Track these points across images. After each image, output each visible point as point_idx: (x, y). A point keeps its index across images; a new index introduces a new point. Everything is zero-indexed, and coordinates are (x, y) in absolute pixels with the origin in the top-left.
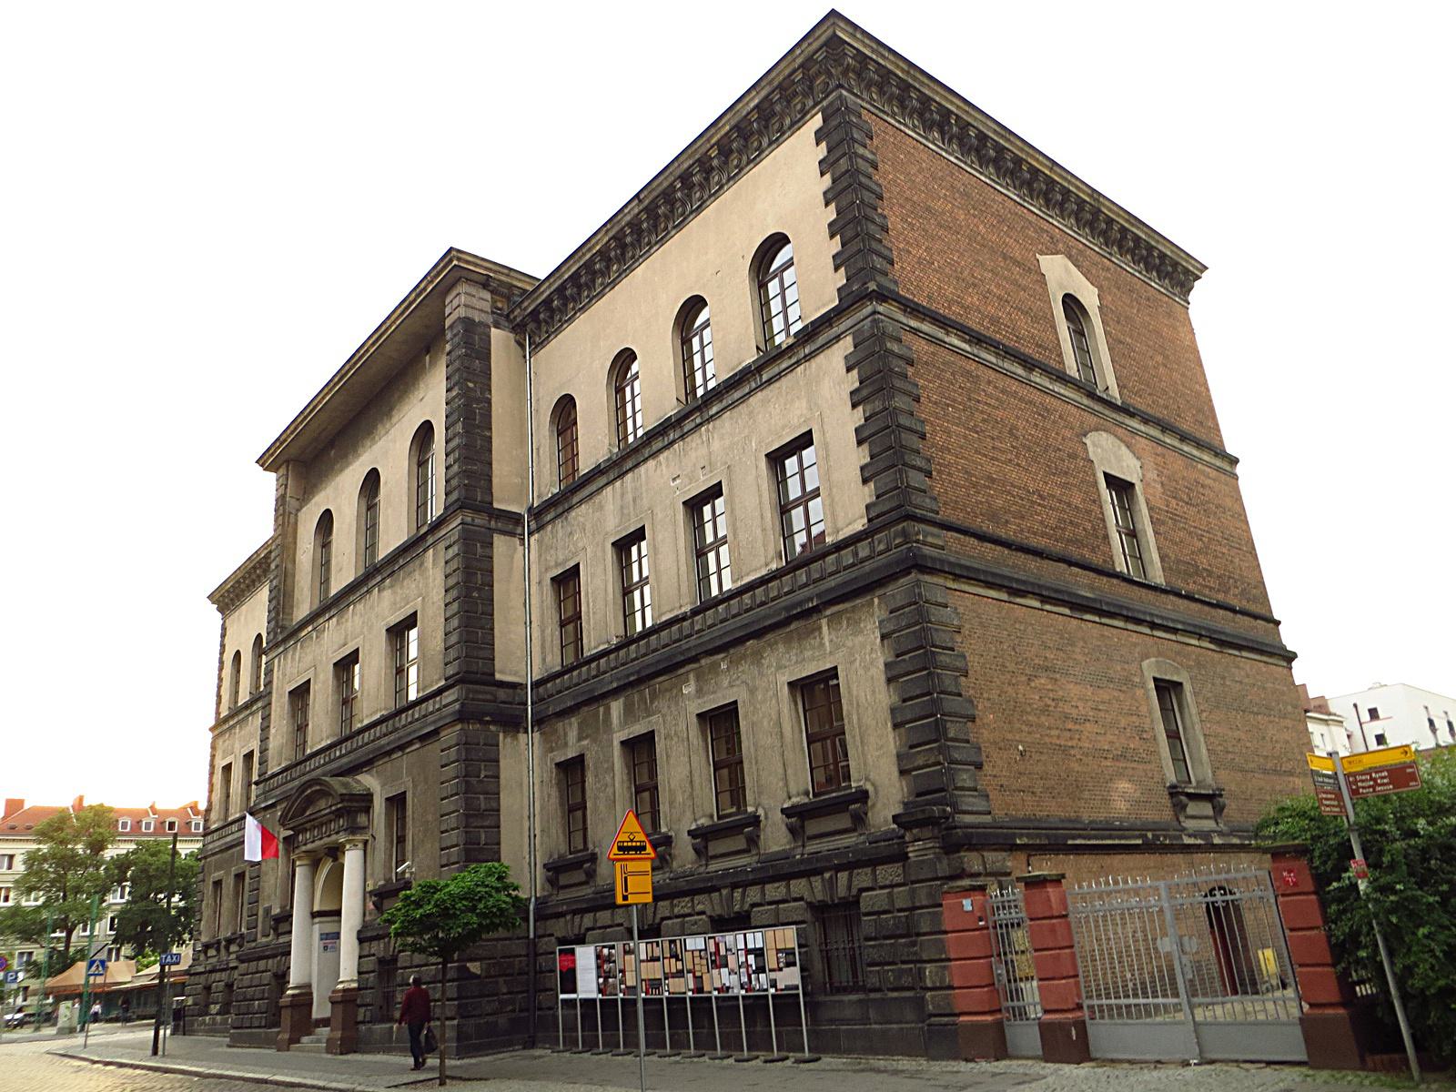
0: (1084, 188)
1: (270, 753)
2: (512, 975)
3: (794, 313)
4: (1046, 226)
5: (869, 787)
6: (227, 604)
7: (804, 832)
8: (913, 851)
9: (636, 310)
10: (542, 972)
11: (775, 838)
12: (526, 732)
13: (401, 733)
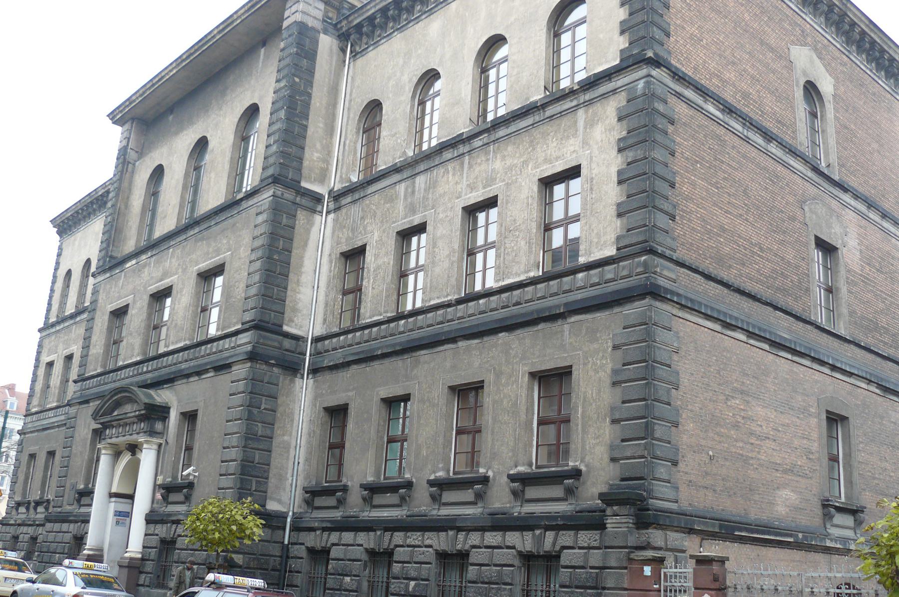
2: (267, 570)
3: (581, 63)
4: (799, 21)
5: (583, 468)
6: (65, 229)
7: (524, 494)
8: (610, 522)
12: (302, 378)
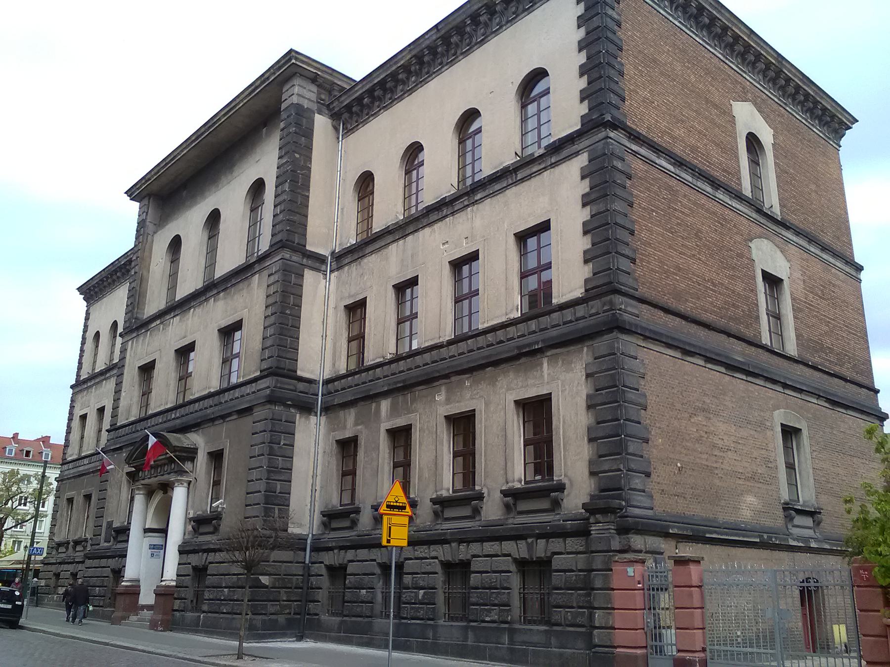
0: (772, 52)
1: (120, 410)
2: (291, 588)
4: (740, 79)
5: (566, 481)
9: (426, 114)
10: (312, 588)
11: (492, 510)
13: (224, 406)
